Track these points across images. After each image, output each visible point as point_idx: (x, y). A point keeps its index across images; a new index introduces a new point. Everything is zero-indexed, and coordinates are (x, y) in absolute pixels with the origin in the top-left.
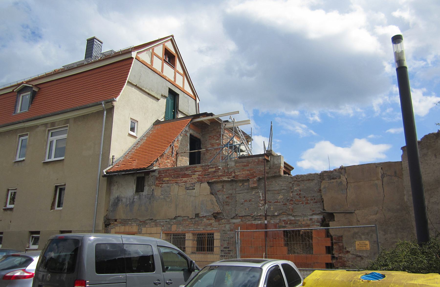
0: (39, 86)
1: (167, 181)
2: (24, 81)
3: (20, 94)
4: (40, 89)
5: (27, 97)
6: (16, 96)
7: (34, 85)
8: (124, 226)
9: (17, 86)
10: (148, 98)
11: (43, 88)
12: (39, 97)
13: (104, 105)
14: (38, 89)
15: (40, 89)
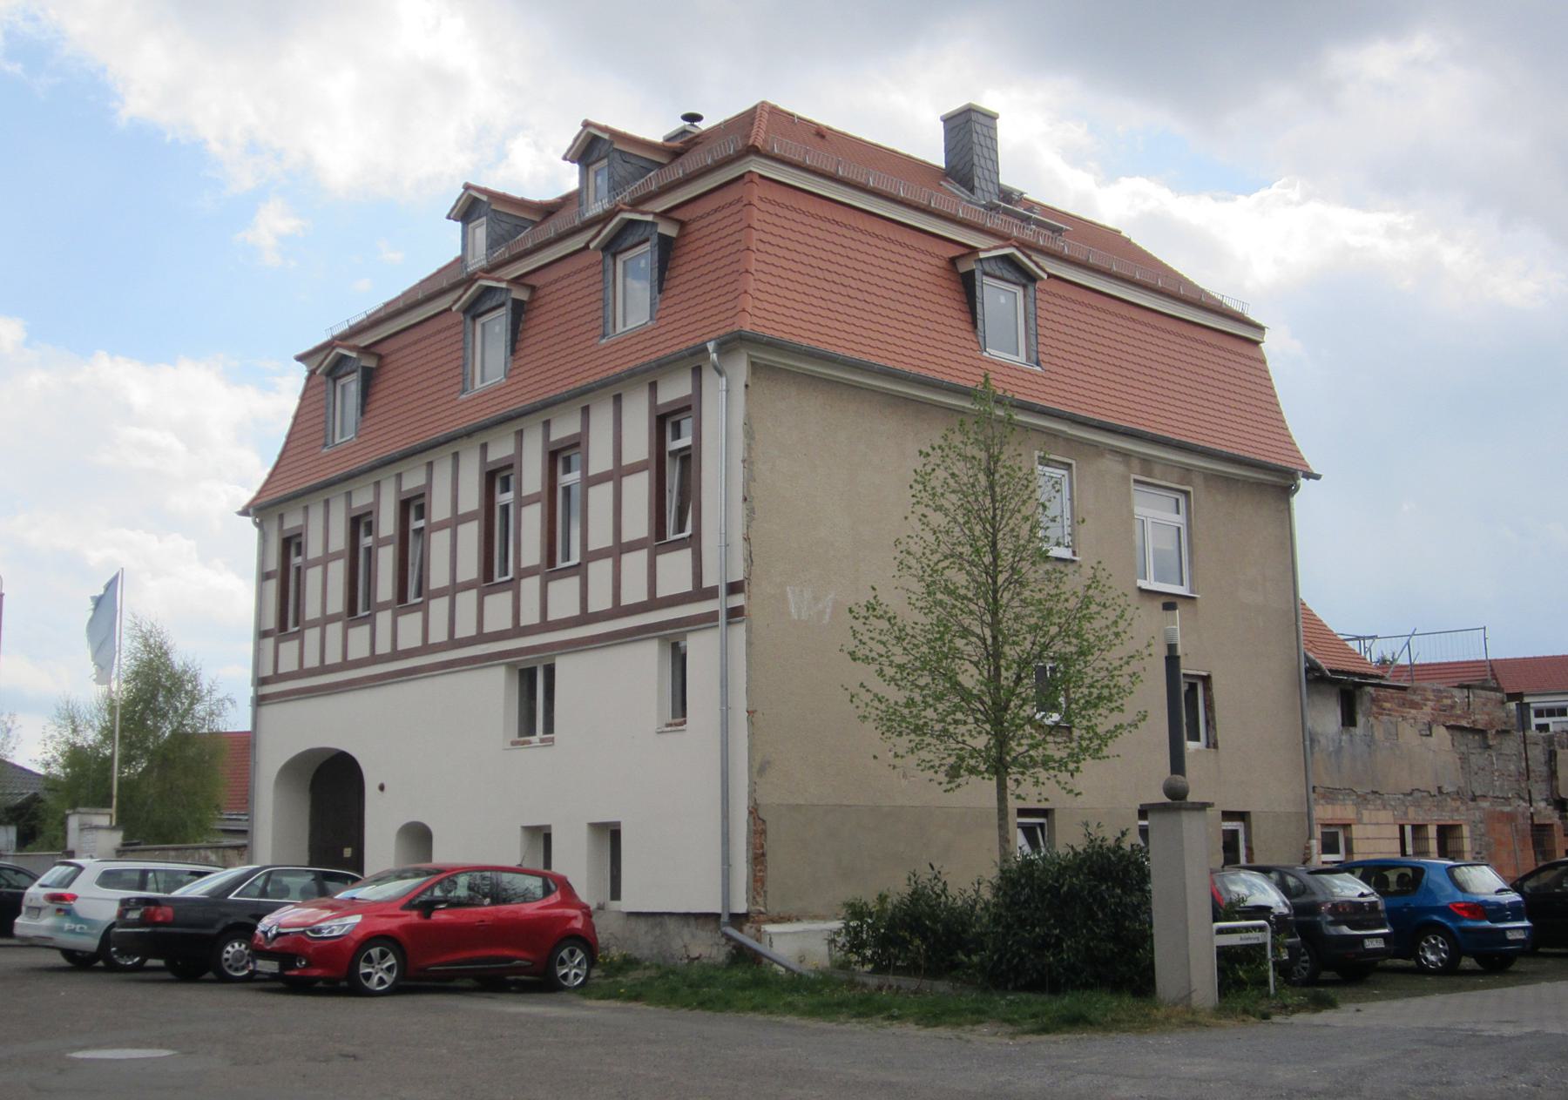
0: (677, 215)
1: (1389, 710)
2: (624, 204)
3: (614, 256)
4: (682, 224)
5: (643, 263)
6: (600, 267)
7: (658, 211)
8: (1333, 804)
9: (327, 351)
10: (1100, 264)
11: (545, 286)
12: (685, 259)
13: (715, 355)
14: (678, 227)
15: (682, 224)
